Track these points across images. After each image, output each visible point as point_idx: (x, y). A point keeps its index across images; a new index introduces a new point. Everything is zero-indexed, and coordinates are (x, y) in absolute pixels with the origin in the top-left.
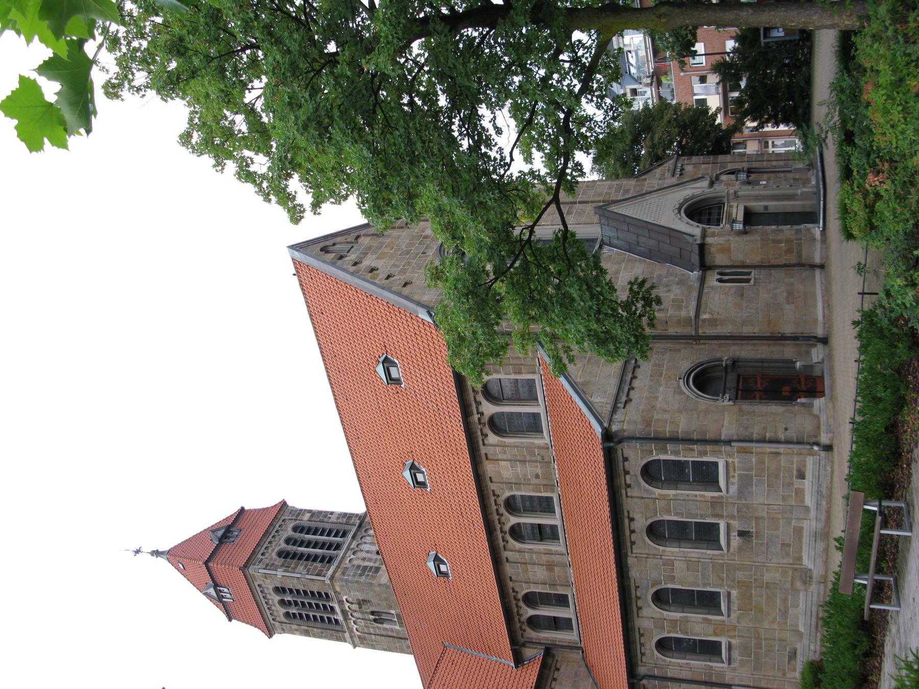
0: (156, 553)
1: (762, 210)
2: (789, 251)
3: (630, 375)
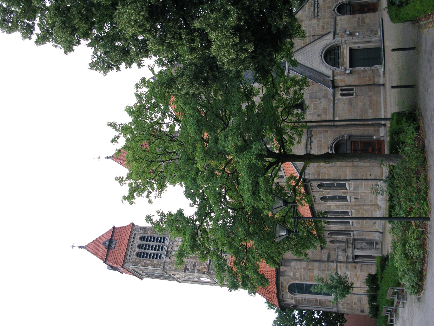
0: (107, 158)
1: (357, 48)
2: (370, 80)
3: (309, 148)
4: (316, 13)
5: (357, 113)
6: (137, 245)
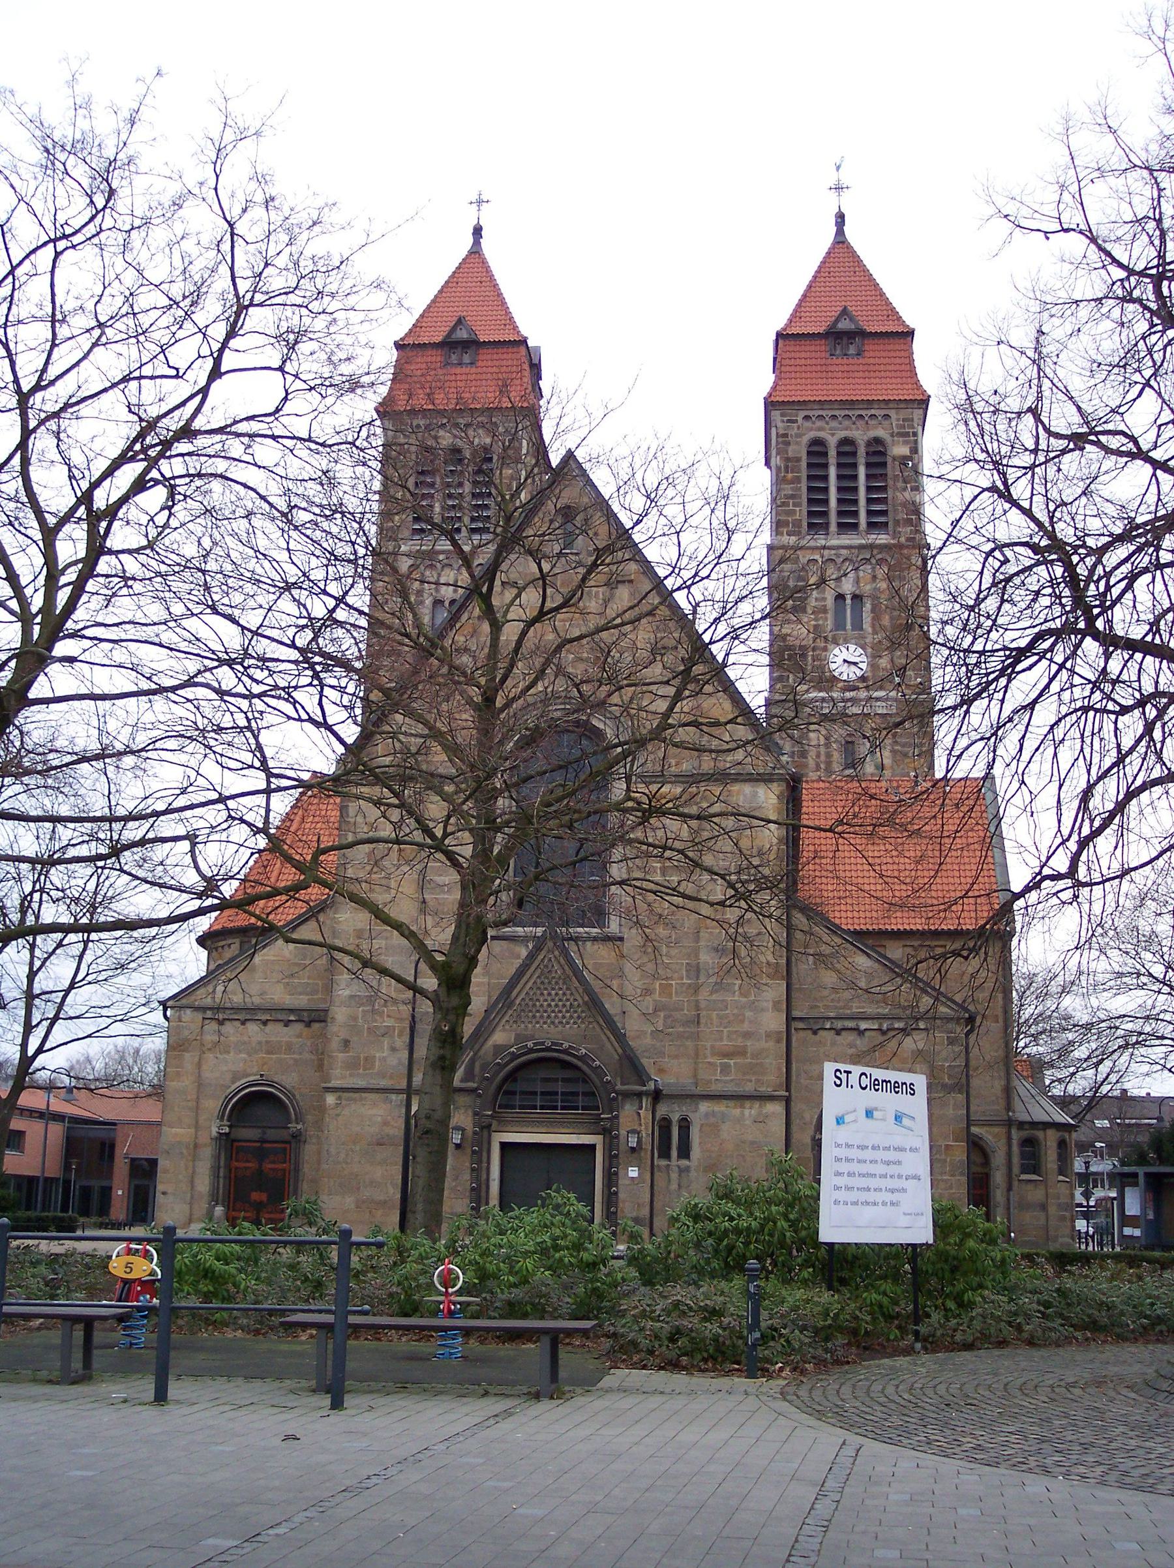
4: (851, 1024)
5: (347, 1163)
6: (821, 434)
